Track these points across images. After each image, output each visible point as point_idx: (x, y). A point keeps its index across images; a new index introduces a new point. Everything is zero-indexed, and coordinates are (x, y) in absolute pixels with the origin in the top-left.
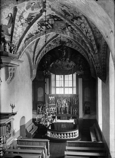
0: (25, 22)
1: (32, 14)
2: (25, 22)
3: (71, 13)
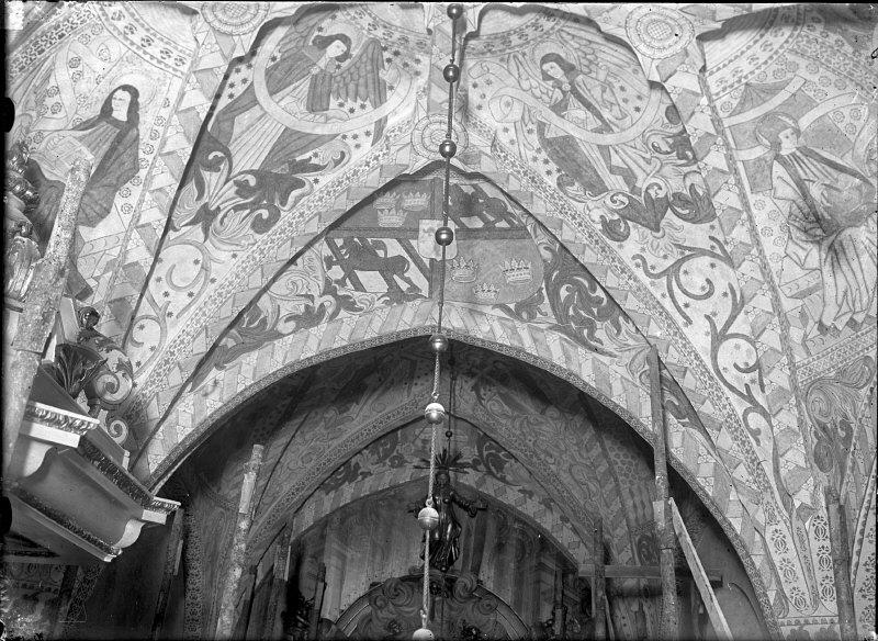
0: (237, 208)
1: (304, 149)
2: (237, 208)
3: (612, 170)
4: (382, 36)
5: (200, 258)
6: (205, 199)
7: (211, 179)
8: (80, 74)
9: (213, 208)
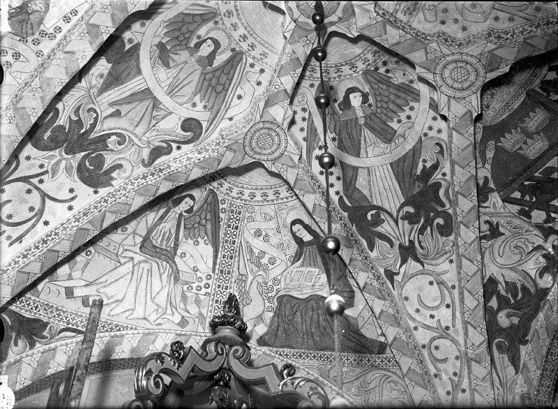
0: (422, 231)
1: (414, 165)
2: (422, 231)
4: (365, 66)
5: (432, 279)
6: (397, 243)
7: (386, 228)
8: (267, 235)
9: (407, 244)
